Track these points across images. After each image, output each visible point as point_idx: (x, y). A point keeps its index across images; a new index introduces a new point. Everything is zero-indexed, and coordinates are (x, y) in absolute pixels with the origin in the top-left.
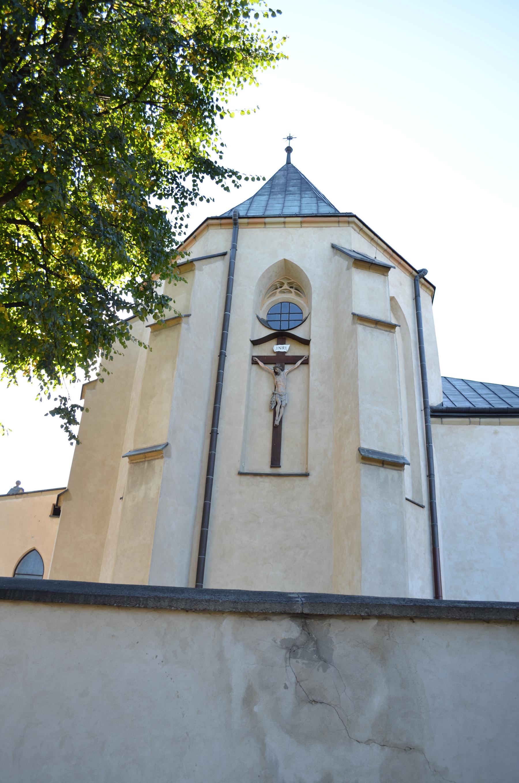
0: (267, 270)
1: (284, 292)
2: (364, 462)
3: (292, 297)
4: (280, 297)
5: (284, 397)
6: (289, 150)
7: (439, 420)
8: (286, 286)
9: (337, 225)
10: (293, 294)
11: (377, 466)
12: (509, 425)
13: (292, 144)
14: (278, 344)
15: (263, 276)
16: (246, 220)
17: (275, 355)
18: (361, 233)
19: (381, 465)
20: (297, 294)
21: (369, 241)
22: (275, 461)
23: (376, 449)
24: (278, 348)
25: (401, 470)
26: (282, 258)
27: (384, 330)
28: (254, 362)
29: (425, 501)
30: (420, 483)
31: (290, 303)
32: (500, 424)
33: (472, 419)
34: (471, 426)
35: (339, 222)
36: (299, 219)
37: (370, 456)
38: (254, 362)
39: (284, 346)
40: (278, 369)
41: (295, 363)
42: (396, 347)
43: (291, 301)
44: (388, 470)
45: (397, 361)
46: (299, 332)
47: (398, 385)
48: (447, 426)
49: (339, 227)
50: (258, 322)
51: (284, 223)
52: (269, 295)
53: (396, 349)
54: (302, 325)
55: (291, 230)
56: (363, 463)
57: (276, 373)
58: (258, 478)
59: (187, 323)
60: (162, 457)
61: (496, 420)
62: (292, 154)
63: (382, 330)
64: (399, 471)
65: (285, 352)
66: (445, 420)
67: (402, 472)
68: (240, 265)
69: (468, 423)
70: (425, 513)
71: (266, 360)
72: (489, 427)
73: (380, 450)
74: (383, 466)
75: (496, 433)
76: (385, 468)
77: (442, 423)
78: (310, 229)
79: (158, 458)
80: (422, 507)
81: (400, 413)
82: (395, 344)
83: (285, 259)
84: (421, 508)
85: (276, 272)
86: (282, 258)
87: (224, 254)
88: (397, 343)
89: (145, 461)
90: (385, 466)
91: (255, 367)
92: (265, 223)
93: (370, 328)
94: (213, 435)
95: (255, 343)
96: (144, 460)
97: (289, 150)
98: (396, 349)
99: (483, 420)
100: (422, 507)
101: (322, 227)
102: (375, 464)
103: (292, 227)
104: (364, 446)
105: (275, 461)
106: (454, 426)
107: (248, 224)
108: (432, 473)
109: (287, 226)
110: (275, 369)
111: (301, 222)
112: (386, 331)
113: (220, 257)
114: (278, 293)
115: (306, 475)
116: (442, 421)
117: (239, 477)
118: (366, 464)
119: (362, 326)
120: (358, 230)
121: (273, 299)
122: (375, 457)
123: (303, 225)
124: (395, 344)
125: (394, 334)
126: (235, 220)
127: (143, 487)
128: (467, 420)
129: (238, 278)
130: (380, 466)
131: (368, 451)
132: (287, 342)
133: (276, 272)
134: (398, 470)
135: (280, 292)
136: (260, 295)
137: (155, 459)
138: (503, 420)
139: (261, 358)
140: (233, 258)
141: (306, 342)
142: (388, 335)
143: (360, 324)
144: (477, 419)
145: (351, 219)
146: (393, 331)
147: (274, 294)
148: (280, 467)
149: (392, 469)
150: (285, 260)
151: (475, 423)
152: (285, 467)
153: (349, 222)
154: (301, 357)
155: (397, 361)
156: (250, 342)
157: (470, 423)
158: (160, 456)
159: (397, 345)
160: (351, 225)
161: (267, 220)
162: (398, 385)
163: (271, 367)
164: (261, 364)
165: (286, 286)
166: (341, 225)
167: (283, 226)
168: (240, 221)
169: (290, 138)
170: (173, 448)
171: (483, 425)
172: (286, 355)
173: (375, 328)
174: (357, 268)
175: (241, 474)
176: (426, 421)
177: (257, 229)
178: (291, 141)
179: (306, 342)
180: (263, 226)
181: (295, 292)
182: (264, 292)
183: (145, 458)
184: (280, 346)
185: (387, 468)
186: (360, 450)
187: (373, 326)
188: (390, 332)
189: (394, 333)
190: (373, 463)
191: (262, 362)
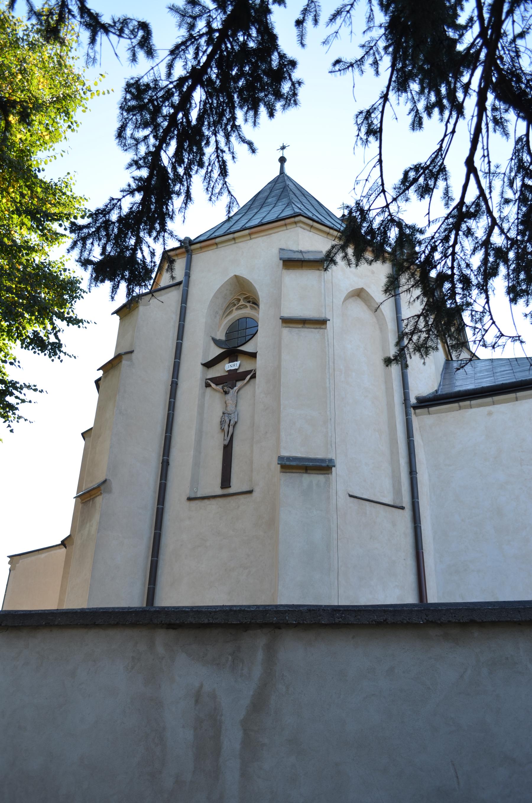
0: (218, 290)
1: (241, 308)
2: (284, 470)
3: (247, 312)
4: (236, 314)
5: (233, 415)
6: (282, 160)
7: (426, 410)
8: (242, 302)
9: (285, 228)
10: (249, 308)
11: (300, 473)
12: (505, 403)
13: (286, 153)
14: (229, 363)
15: (215, 296)
16: (198, 246)
17: (227, 374)
18: (312, 230)
19: (304, 471)
20: (252, 308)
21: (326, 236)
22: (226, 482)
23: (299, 455)
24: (229, 366)
25: (328, 474)
26: (232, 275)
27: (314, 328)
28: (208, 385)
29: (406, 501)
30: (400, 483)
31: (246, 318)
32: (494, 403)
33: (462, 404)
34: (461, 411)
35: (286, 225)
36: (247, 232)
37: (292, 463)
38: (208, 385)
39: (235, 363)
40: (226, 388)
41: (244, 379)
42: (327, 343)
43: (247, 316)
44: (312, 475)
45: (327, 358)
46: (248, 348)
47: (328, 383)
48: (435, 415)
49: (287, 229)
50: (212, 344)
51: (234, 239)
52: (226, 314)
53: (327, 345)
54: (254, 338)
55: (241, 245)
56: (283, 472)
57: (226, 393)
58: (206, 502)
59: (130, 360)
60: (101, 494)
61: (489, 400)
62: (286, 165)
63: (311, 328)
64: (327, 475)
65: (237, 369)
66: (432, 409)
67: (330, 475)
68: (194, 291)
69: (458, 408)
70: (407, 514)
71: (217, 381)
72: (481, 409)
73: (304, 456)
74: (306, 473)
75: (490, 414)
76: (309, 473)
77: (429, 413)
78: (260, 238)
79: (99, 495)
80: (402, 508)
81: (328, 413)
82: (326, 340)
83: (235, 276)
84: (401, 511)
85: (230, 290)
86: (232, 275)
87: (179, 283)
88: (328, 339)
89: (90, 500)
90: (308, 471)
91: (209, 389)
92: (216, 244)
93: (297, 329)
94: (165, 465)
95: (208, 365)
96: (89, 499)
97: (282, 160)
98: (327, 345)
99: (473, 402)
100: (402, 508)
101: (271, 234)
102: (297, 471)
103: (242, 241)
104: (285, 453)
105: (226, 482)
106: (443, 414)
107: (201, 248)
108: (414, 469)
109: (237, 241)
110: (223, 388)
111: (250, 234)
112: (317, 328)
113: (173, 288)
114: (234, 310)
115: (250, 492)
116: (429, 411)
117: (188, 503)
118: (286, 472)
119: (287, 329)
120: (309, 228)
121: (230, 317)
122: (294, 463)
123: (253, 236)
124: (326, 340)
125: (326, 330)
126: (186, 247)
127: (88, 525)
128: (456, 405)
129: (191, 304)
130: (303, 473)
131: (288, 458)
132: (238, 359)
133: (230, 290)
134: (324, 474)
135: (237, 309)
136: (216, 317)
137: (97, 496)
138: (496, 398)
139: (213, 380)
140: (187, 285)
141: (253, 355)
142: (318, 332)
143: (286, 327)
144: (468, 403)
145: (297, 219)
146: (323, 327)
147: (231, 312)
148: (230, 487)
149: (318, 474)
150: (236, 276)
151: (466, 407)
152: (236, 486)
153: (296, 223)
154: (251, 371)
155: (327, 358)
156: (201, 366)
157: (460, 408)
158: (99, 493)
159: (328, 341)
160: (298, 225)
161: (218, 240)
162: (328, 383)
163: (219, 388)
164: (213, 385)
165: (242, 302)
166: (289, 227)
167: (233, 242)
168: (193, 247)
169: (283, 148)
170: (115, 485)
171: (475, 407)
172: (238, 371)
173: (303, 327)
174: (289, 269)
175: (190, 499)
176: (407, 414)
177: (210, 252)
178: (285, 150)
179: (253, 355)
180: (215, 247)
181: (251, 306)
182: (221, 312)
183: (91, 496)
184: (231, 364)
185: (312, 474)
186: (281, 458)
187: (300, 326)
188: (320, 328)
189: (326, 328)
190: (294, 471)
191: (214, 383)
